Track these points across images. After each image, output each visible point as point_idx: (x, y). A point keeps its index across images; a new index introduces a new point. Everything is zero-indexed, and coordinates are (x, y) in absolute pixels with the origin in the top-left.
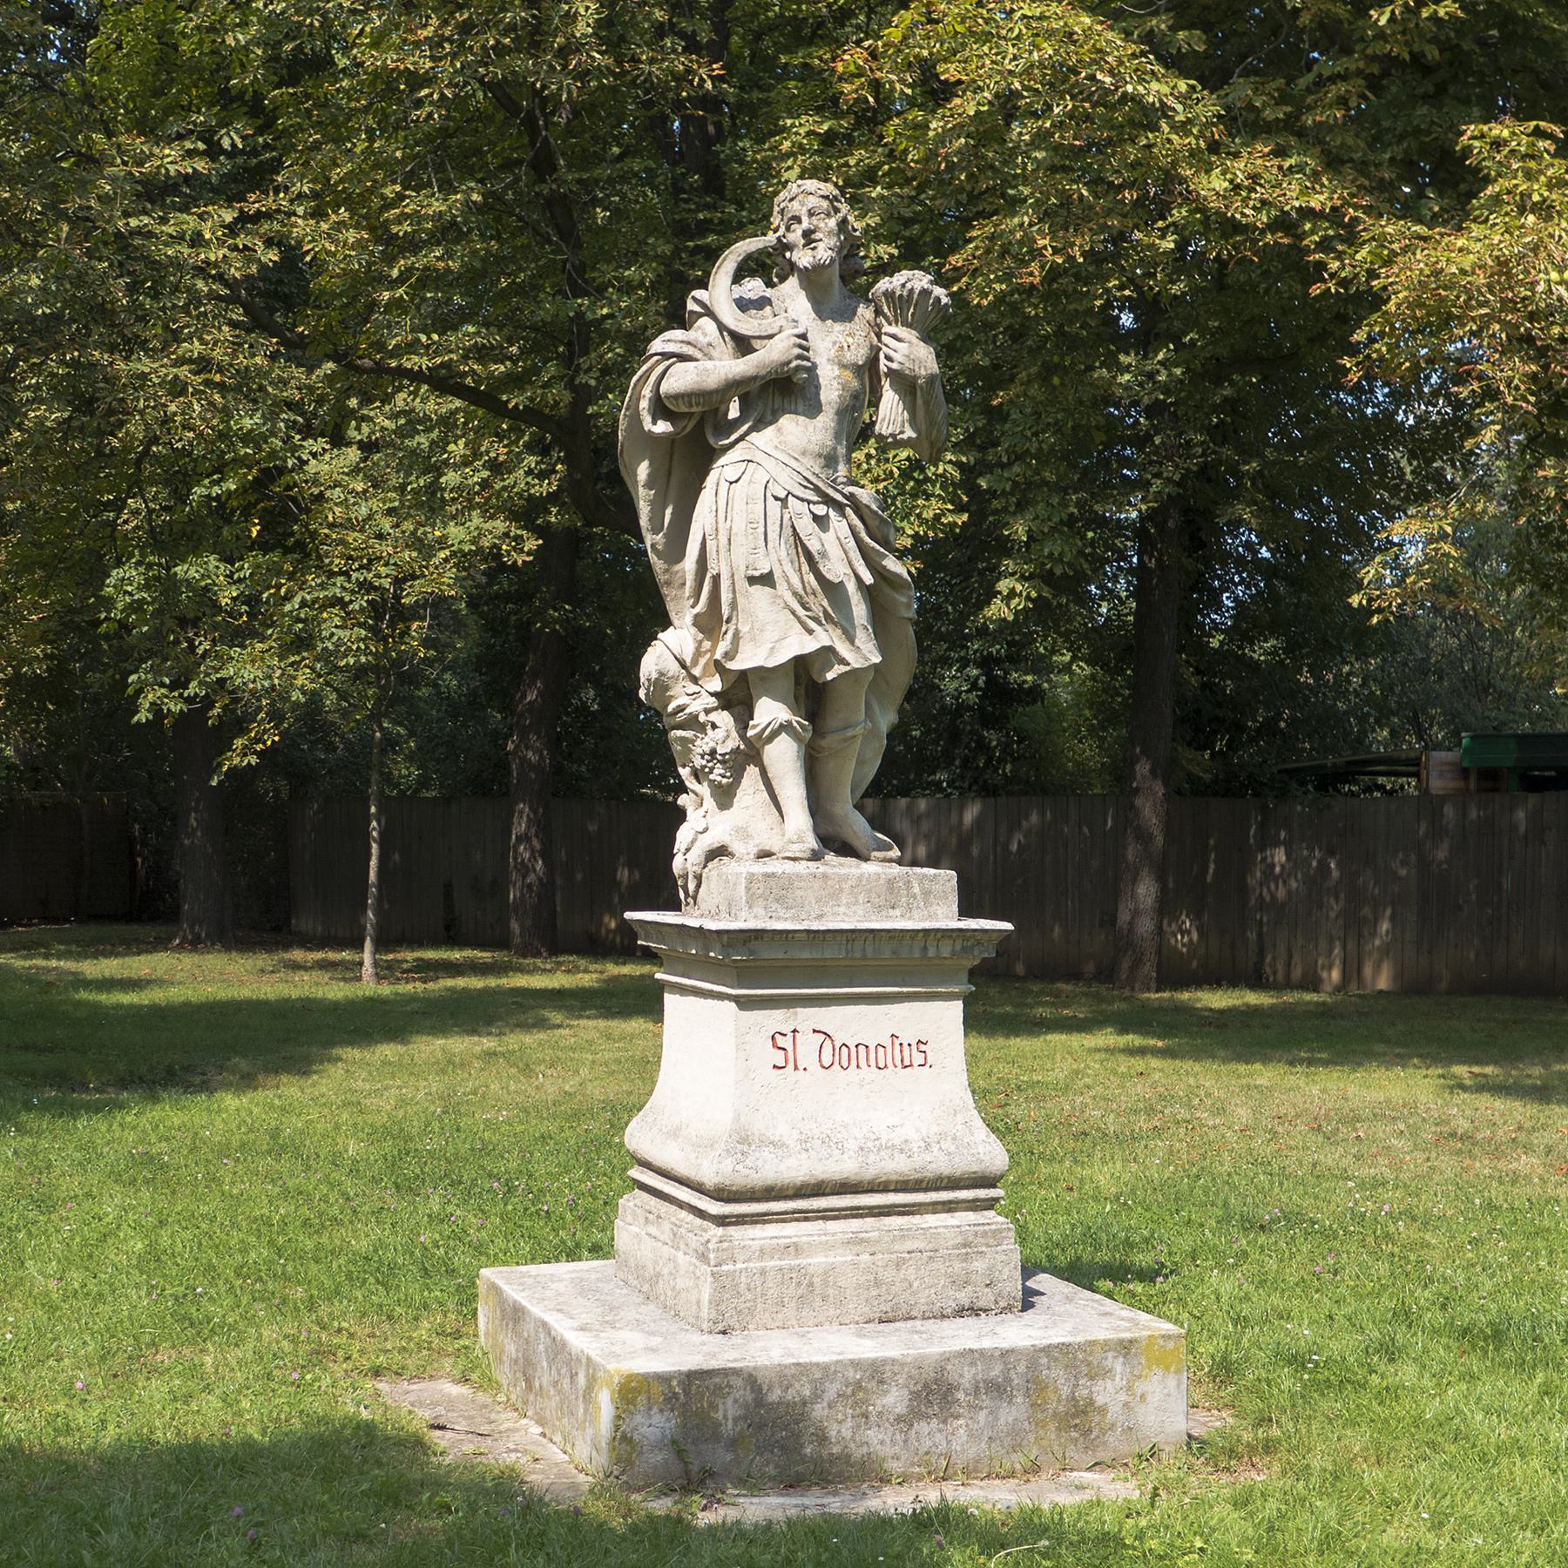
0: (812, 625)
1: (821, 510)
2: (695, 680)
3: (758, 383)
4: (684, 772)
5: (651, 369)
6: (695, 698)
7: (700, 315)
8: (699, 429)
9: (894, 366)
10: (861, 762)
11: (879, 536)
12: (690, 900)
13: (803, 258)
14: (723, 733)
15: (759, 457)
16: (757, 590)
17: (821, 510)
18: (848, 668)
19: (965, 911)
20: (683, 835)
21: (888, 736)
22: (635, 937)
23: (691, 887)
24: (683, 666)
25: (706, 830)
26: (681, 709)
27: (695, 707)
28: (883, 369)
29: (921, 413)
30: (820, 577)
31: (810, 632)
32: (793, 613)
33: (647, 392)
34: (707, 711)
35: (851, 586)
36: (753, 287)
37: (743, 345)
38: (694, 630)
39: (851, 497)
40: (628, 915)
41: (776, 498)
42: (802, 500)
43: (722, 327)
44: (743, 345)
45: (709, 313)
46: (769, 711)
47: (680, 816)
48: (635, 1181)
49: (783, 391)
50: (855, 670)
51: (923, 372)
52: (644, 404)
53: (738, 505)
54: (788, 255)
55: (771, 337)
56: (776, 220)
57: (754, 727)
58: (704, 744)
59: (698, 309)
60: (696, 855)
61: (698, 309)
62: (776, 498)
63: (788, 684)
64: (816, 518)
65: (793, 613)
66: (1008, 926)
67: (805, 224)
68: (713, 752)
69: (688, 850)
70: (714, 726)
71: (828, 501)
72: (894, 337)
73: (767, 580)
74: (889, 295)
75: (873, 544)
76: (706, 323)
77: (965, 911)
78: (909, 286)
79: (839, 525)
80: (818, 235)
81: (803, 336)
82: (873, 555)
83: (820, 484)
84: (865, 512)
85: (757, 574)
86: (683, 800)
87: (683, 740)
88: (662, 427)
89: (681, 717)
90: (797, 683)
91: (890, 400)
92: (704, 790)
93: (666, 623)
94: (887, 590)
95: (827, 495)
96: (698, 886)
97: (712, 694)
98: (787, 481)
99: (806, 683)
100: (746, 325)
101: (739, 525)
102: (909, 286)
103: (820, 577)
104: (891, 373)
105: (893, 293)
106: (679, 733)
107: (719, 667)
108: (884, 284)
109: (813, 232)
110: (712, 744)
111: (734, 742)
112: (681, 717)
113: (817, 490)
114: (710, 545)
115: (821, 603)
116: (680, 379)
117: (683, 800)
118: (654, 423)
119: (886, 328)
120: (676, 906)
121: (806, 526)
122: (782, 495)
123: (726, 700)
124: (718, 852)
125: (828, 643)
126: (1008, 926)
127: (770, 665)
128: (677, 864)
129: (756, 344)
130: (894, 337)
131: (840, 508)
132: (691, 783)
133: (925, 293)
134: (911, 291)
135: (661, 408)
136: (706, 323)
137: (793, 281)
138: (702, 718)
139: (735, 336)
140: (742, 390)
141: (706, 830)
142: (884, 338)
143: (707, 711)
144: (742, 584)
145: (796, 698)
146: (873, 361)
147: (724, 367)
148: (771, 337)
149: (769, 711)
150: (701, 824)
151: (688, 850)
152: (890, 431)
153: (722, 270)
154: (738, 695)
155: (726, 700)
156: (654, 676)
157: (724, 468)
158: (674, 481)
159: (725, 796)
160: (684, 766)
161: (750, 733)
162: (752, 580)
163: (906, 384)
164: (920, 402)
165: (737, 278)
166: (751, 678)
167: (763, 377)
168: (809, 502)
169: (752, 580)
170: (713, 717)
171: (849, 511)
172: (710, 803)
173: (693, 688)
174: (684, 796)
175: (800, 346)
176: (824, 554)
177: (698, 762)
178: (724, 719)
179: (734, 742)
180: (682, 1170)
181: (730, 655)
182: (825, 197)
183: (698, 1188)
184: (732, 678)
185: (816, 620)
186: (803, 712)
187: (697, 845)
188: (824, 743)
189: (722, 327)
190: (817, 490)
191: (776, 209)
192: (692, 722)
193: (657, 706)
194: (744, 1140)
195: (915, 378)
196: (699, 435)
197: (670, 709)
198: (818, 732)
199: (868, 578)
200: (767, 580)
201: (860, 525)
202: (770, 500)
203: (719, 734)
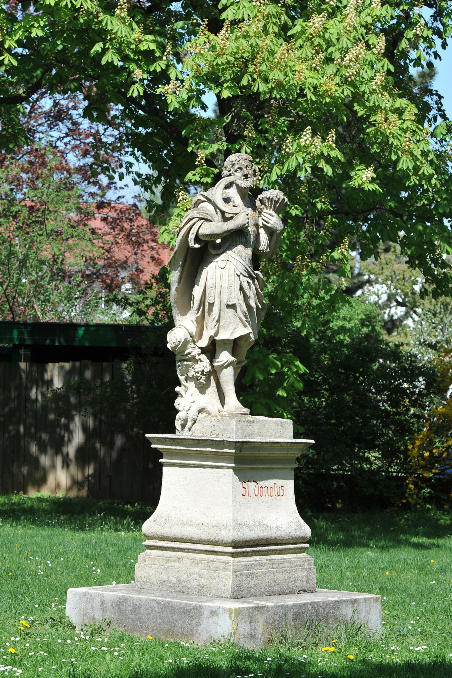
15: (231, 259)
16: (231, 311)
19: (296, 435)
22: (150, 444)
26: (189, 353)
29: (273, 243)
31: (246, 326)
32: (240, 319)
34: (199, 355)
39: (257, 275)
40: (147, 435)
46: (225, 357)
48: (146, 546)
63: (231, 346)
65: (240, 319)
66: (313, 441)
71: (250, 276)
73: (233, 307)
85: (230, 304)
88: (197, 246)
89: (189, 356)
98: (241, 269)
111: (209, 368)
112: (189, 356)
120: (174, 433)
121: (245, 286)
126: (313, 441)
134: (279, 199)
149: (225, 357)
160: (182, 375)
162: (228, 306)
169: (228, 306)
173: (193, 345)
178: (203, 357)
179: (209, 368)
180: (204, 536)
183: (224, 544)
194: (238, 525)
195: (277, 230)
200: (233, 307)
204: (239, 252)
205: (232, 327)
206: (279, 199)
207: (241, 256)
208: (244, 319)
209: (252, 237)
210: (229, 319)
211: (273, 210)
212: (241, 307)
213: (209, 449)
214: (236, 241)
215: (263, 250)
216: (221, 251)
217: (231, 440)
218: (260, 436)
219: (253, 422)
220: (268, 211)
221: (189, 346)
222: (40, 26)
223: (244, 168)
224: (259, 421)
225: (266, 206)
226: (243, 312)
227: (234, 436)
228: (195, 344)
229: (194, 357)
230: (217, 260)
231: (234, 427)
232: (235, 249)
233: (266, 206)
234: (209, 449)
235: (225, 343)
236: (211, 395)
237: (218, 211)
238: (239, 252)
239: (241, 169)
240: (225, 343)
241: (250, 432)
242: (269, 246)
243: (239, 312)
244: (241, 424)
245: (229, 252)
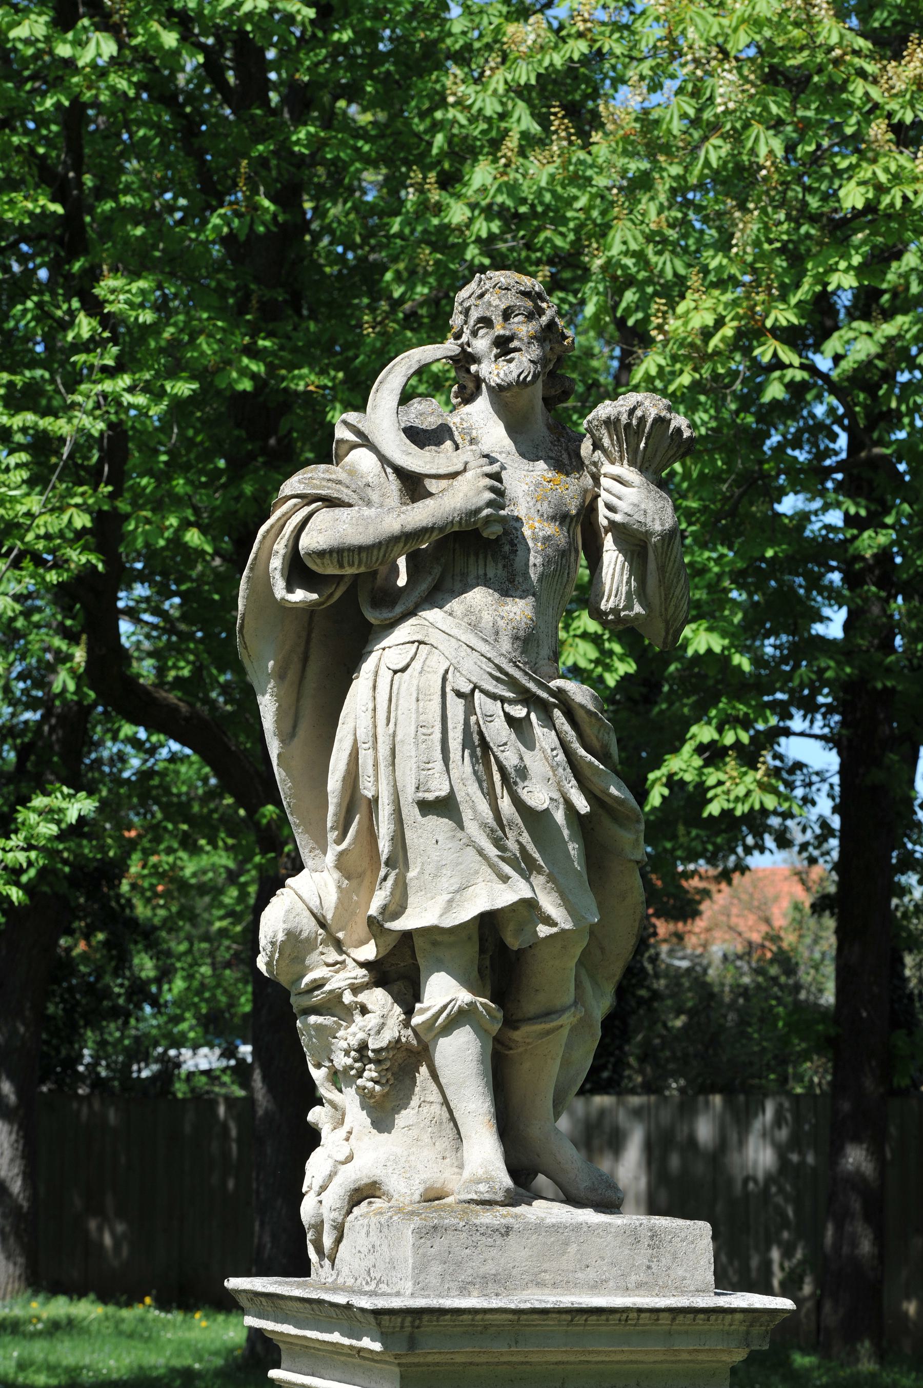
0: (507, 869)
1: (519, 712)
2: (339, 946)
3: (435, 536)
4: (318, 1075)
5: (287, 517)
6: (336, 972)
7: (355, 446)
8: (351, 595)
9: (618, 518)
10: (566, 1063)
11: (596, 744)
12: (327, 1262)
13: (493, 371)
14: (379, 1018)
15: (434, 637)
16: (439, 825)
17: (519, 712)
18: (554, 930)
19: (725, 1280)
20: (316, 1166)
21: (603, 1023)
23: (328, 1241)
24: (322, 924)
25: (349, 1159)
26: (318, 985)
27: (338, 981)
28: (603, 522)
30: (518, 802)
31: (505, 879)
32: (481, 852)
33: (281, 547)
34: (356, 989)
35: (559, 816)
36: (427, 412)
37: (413, 486)
38: (336, 875)
39: (560, 694)
41: (459, 694)
42: (494, 697)
43: (384, 460)
44: (413, 486)
45: (365, 441)
46: (442, 991)
47: (313, 1138)
49: (468, 552)
50: (563, 931)
51: (658, 527)
52: (276, 563)
53: (406, 703)
54: (473, 368)
55: (453, 475)
56: (456, 320)
57: (423, 1011)
58: (351, 1034)
59: (351, 437)
60: (334, 1196)
61: (351, 437)
62: (459, 694)
64: (511, 720)
65: (481, 852)
67: (499, 330)
68: (363, 1047)
69: (323, 1188)
70: (364, 1011)
71: (527, 698)
72: (618, 480)
73: (444, 807)
74: (611, 423)
75: (590, 757)
76: (362, 459)
77: (725, 1280)
78: (639, 413)
79: (545, 737)
80: (515, 344)
81: (497, 477)
82: (588, 772)
83: (517, 674)
84: (581, 715)
85: (430, 797)
86: (315, 1115)
87: (319, 1028)
88: (299, 595)
89: (318, 996)
90: (482, 951)
91: (612, 557)
92: (349, 1099)
93: (297, 867)
94: (607, 822)
95: (527, 690)
96: (339, 1240)
97: (362, 965)
98: (472, 670)
99: (495, 951)
100: (417, 460)
101: (406, 731)
102: (639, 413)
103: (518, 802)
104: (613, 526)
105: (618, 420)
106: (313, 1019)
107: (375, 927)
108: (605, 410)
109: (511, 338)
110: (361, 1035)
112: (318, 996)
113: (512, 683)
114: (366, 757)
115: (520, 837)
116: (324, 532)
117: (315, 1115)
118: (290, 589)
119: (607, 468)
120: (301, 1268)
121: (498, 731)
122: (466, 688)
123: (380, 973)
124: (362, 1194)
125: (528, 894)
127: (450, 921)
128: (307, 1209)
129: (432, 486)
130: (618, 480)
131: (544, 710)
132: (325, 1090)
133: (661, 421)
134: (642, 419)
135: (299, 570)
136: (362, 459)
137: (482, 403)
138: (348, 998)
139: (399, 471)
140: (411, 548)
141: (349, 1159)
142: (604, 481)
143: (356, 989)
144: (411, 813)
145: (480, 971)
146: (589, 510)
147: (393, 516)
148: (453, 475)
150: (345, 1148)
151: (323, 1188)
152: (611, 605)
153: (387, 386)
154: (399, 969)
155: (380, 973)
156: (281, 937)
157: (389, 651)
158: (314, 668)
159: (382, 1113)
160: (318, 1066)
161: (416, 1020)
162: (426, 807)
163: (633, 541)
164: (652, 565)
165: (405, 398)
166: (418, 942)
167: (441, 529)
168: (503, 700)
169: (426, 807)
170: (362, 997)
171: (557, 713)
172: (357, 1117)
173: (333, 956)
174: (317, 1109)
175: (492, 489)
176: (523, 772)
177: (341, 1061)
178: (378, 998)
181: (396, 908)
182: (526, 294)
184: (391, 941)
185: (512, 862)
186: (489, 993)
187: (337, 1181)
188: (517, 1035)
189: (384, 460)
190: (512, 683)
191: (457, 308)
192: (334, 1006)
193: (284, 980)
195: (648, 534)
196: (351, 609)
197: (306, 980)
198: (511, 1022)
199: (582, 805)
200: (444, 807)
201: (570, 734)
202: (450, 695)
203: (371, 1020)
204: (469, 612)
205: (448, 882)
206: (642, 419)
207: (474, 627)
208: (492, 851)
209: (535, 559)
210: (435, 856)
211: (632, 463)
212: (474, 809)
213: (336, 1337)
214: (464, 575)
215: (615, 611)
216: (399, 610)
217: (396, 1303)
218: (540, 1284)
219: (507, 1231)
220: (616, 469)
221: (313, 958)
222: (850, 267)
223: (497, 320)
224: (539, 1227)
225: (604, 451)
226: (484, 825)
227: (408, 1286)
228: (341, 951)
229: (337, 996)
230: (384, 643)
231: (409, 1252)
232: (456, 605)
233: (604, 451)
234: (336, 1337)
235: (435, 944)
236: (414, 1132)
237: (389, 470)
238: (469, 612)
239: (486, 322)
240: (435, 944)
241: (490, 1268)
242: (642, 592)
243: (472, 828)
244: (440, 1243)
245: (433, 615)
